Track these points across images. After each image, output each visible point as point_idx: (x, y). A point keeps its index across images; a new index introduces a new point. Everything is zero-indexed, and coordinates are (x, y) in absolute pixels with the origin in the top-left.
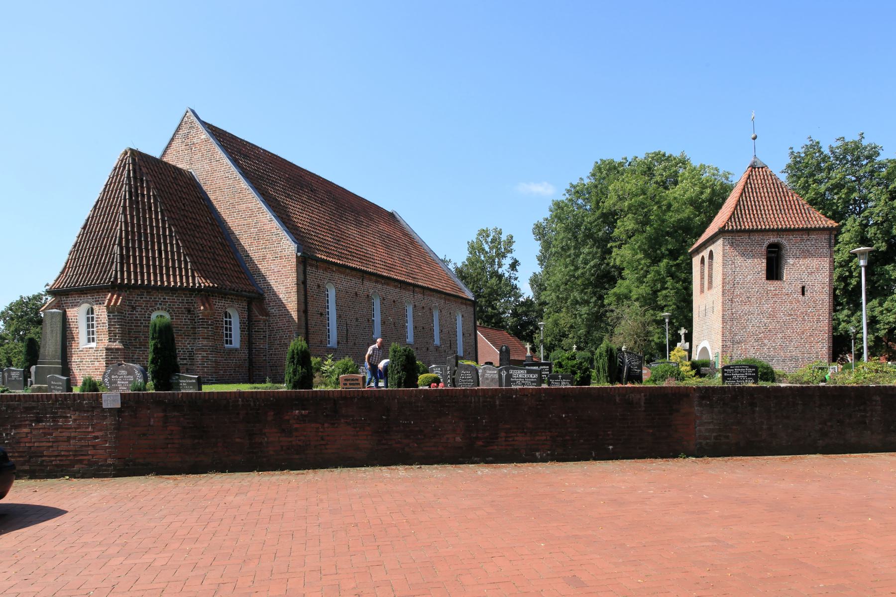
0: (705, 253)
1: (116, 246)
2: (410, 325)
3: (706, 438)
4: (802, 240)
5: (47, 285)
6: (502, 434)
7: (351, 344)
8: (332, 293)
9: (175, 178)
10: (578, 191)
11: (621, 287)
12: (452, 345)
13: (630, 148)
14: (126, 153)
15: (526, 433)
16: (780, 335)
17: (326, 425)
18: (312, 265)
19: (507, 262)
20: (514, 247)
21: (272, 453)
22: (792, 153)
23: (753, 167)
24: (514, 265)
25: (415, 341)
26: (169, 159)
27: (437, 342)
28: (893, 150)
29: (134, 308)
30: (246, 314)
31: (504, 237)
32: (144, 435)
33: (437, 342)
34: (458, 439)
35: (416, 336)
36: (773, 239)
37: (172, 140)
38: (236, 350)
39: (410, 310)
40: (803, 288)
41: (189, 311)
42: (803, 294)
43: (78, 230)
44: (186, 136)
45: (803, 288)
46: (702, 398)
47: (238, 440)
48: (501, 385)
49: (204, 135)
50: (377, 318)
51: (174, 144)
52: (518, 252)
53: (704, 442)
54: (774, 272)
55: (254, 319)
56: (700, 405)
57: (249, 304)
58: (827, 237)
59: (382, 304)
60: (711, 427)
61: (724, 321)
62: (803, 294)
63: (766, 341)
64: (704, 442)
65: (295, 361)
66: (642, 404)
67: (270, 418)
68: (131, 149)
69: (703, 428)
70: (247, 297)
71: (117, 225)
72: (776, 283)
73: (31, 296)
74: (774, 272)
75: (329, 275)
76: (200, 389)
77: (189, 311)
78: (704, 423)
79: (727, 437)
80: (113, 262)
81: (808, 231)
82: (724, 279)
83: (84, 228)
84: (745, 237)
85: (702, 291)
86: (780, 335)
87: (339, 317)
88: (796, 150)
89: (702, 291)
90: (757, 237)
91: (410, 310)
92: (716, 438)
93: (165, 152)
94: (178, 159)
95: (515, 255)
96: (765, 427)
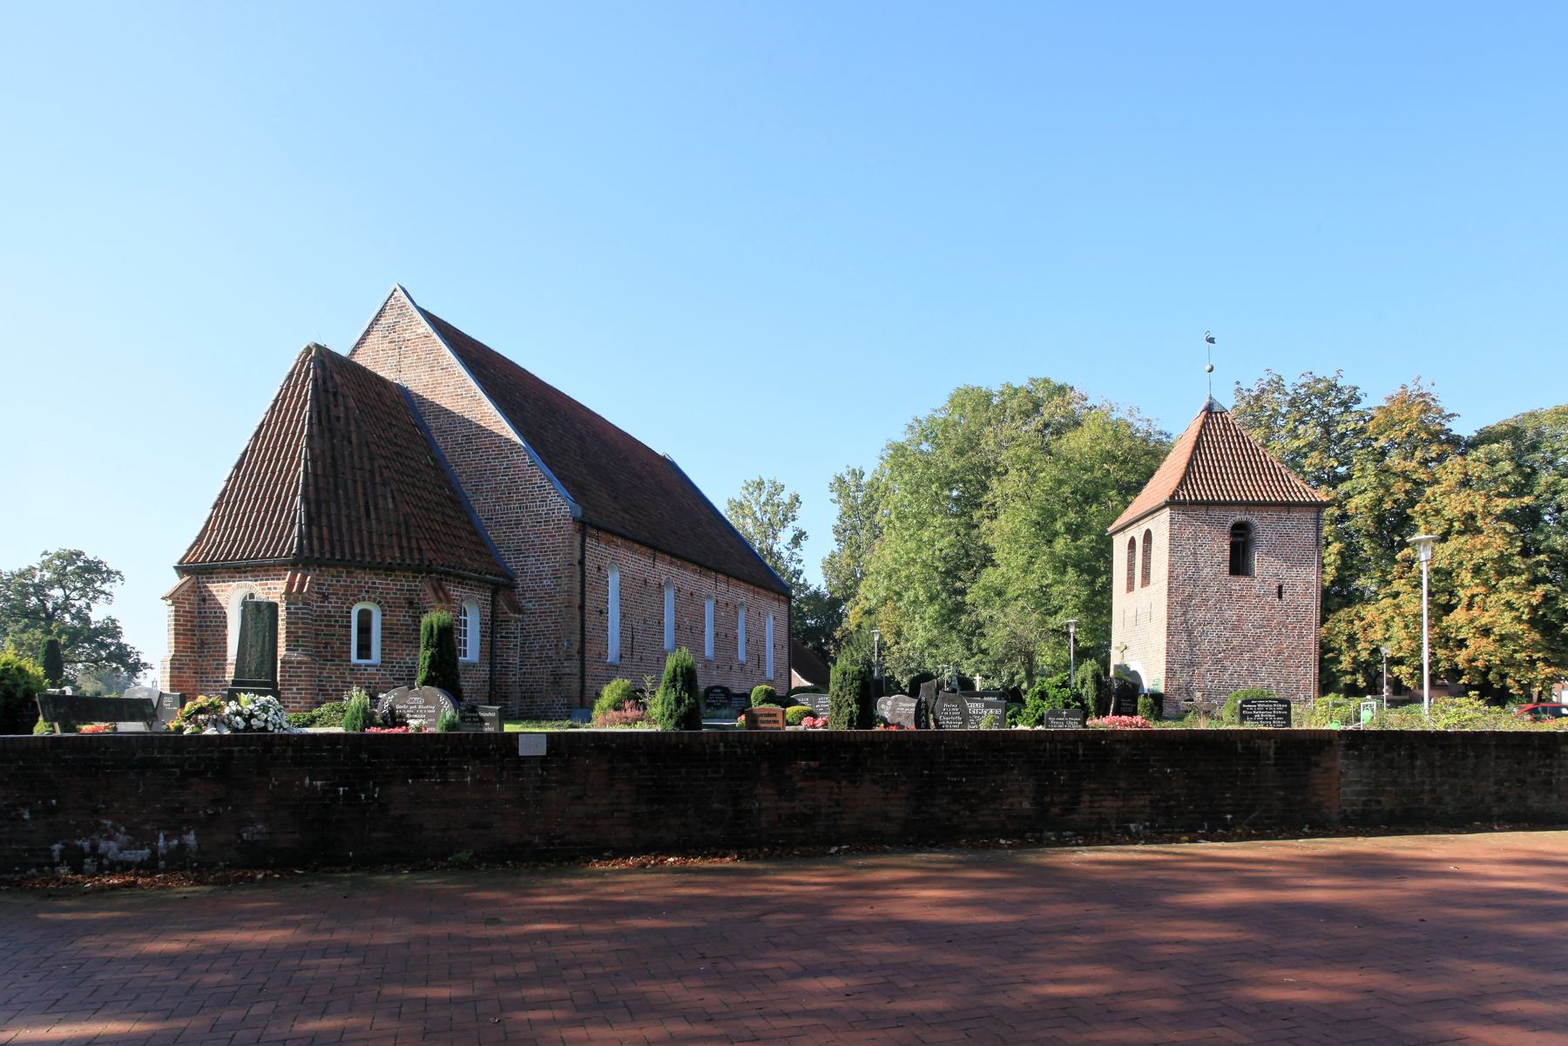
0: (1137, 533)
1: (298, 498)
2: (709, 632)
3: (1353, 804)
4: (1280, 519)
5: (45, 553)
6: (1086, 798)
7: (636, 659)
8: (614, 579)
9: (379, 394)
10: (930, 432)
11: (990, 576)
12: (760, 662)
13: (1004, 370)
14: (309, 350)
15: (1117, 796)
16: (1246, 656)
17: (844, 783)
18: (591, 536)
19: (786, 536)
20: (798, 513)
21: (764, 825)
22: (1239, 390)
23: (1209, 410)
24: (797, 539)
25: (716, 656)
26: (360, 359)
27: (742, 657)
28: (1563, 404)
29: (325, 597)
30: (488, 611)
31: (785, 497)
32: (579, 798)
33: (742, 657)
34: (1026, 805)
35: (716, 649)
36: (1239, 516)
37: (368, 332)
38: (474, 665)
39: (709, 607)
40: (1280, 587)
41: (411, 603)
42: (1280, 597)
43: (228, 470)
44: (392, 328)
45: (1280, 587)
46: (1348, 747)
47: (716, 806)
48: (850, 726)
49: (425, 327)
50: (669, 620)
51: (371, 339)
52: (803, 519)
53: (1349, 810)
54: (1239, 564)
55: (501, 617)
56: (1346, 757)
57: (495, 594)
58: (1314, 515)
59: (677, 597)
60: (1359, 787)
61: (1169, 635)
62: (1280, 597)
63: (1227, 663)
64: (1349, 810)
65: (679, 685)
66: (1271, 753)
67: (764, 773)
68: (317, 346)
69: (1348, 790)
70: (492, 583)
71: (298, 465)
72: (1244, 580)
73: (16, 571)
74: (1239, 564)
75: (612, 551)
76: (501, 728)
77: (411, 603)
78: (1347, 782)
79: (1379, 802)
80: (293, 524)
81: (1289, 506)
82: (1170, 572)
83: (238, 466)
84: (1202, 512)
85: (1130, 588)
86: (1246, 656)
87: (623, 616)
88: (1244, 386)
89: (1130, 588)
90: (1217, 513)
91: (709, 607)
92: (1365, 803)
93: (354, 351)
94: (379, 361)
95: (800, 524)
96: (1427, 788)
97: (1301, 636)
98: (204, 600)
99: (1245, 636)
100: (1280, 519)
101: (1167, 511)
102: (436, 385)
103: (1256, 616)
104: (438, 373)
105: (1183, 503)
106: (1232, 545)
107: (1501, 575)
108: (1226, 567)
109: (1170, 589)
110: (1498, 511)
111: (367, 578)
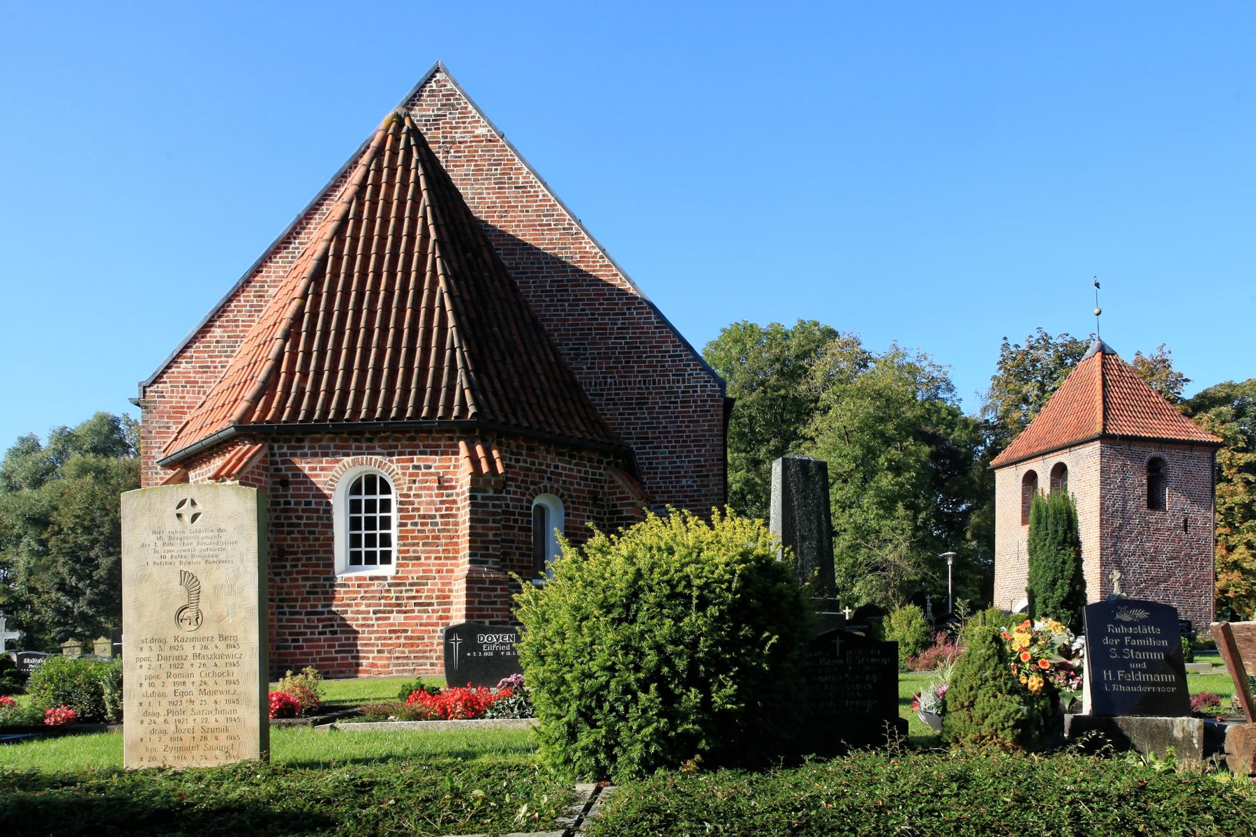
22: (1006, 346)
36: (1154, 453)
40: (1186, 521)
45: (1186, 521)
58: (1209, 455)
61: (1102, 565)
72: (1158, 514)
74: (1154, 502)
82: (1102, 504)
88: (1012, 342)
90: (1137, 448)
97: (1202, 568)
98: (285, 483)
99: (1161, 568)
100: (1184, 457)
101: (1097, 444)
102: (508, 207)
103: (1167, 548)
104: (510, 192)
105: (1113, 437)
106: (1149, 479)
107: (1245, 519)
108: (1143, 501)
109: (1102, 520)
110: (1242, 462)
111: (548, 460)
